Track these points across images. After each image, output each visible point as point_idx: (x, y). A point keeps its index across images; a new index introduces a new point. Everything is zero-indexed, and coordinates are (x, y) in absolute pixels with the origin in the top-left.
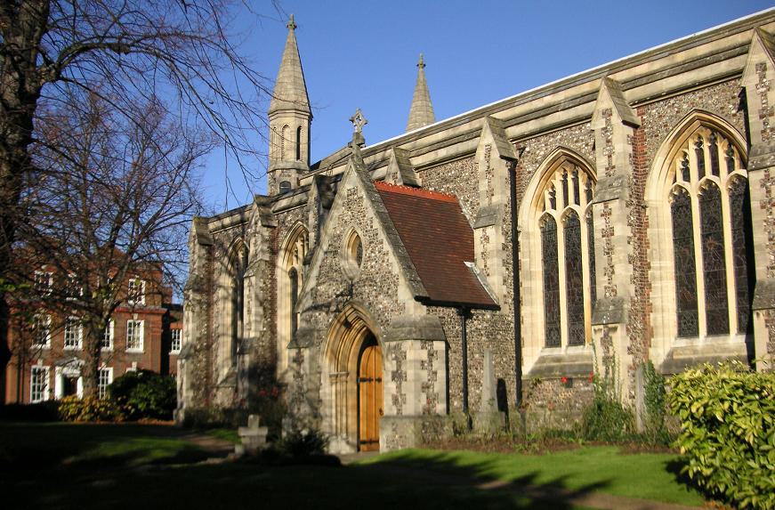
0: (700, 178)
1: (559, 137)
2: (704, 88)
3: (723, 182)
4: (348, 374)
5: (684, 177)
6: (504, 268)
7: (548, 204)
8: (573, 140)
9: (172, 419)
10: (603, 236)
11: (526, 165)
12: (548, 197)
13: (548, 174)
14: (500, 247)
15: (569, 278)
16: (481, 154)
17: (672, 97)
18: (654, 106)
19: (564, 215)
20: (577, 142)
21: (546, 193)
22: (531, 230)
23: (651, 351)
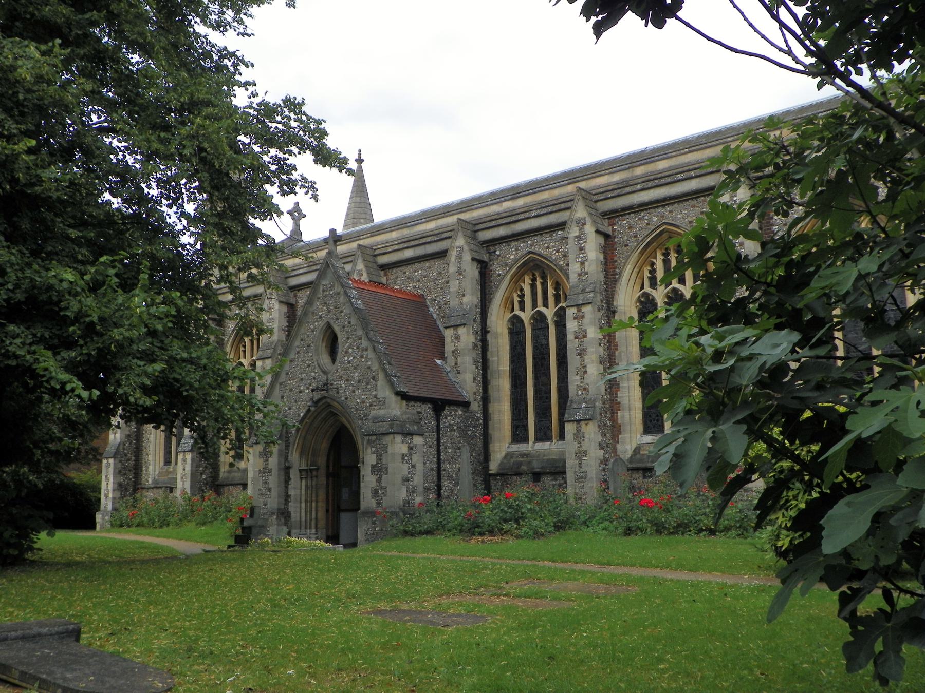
0: (641, 290)
1: (529, 242)
2: (674, 203)
3: (549, 313)
4: (317, 469)
5: (544, 303)
6: (474, 366)
7: (647, 283)
8: (544, 247)
9: (90, 525)
10: (576, 338)
11: (497, 269)
12: (516, 299)
13: (518, 278)
14: (471, 346)
15: (536, 377)
16: (453, 255)
17: (643, 210)
18: (624, 217)
19: (533, 317)
20: (548, 248)
21: (515, 295)
22: (499, 330)
23: (619, 446)
